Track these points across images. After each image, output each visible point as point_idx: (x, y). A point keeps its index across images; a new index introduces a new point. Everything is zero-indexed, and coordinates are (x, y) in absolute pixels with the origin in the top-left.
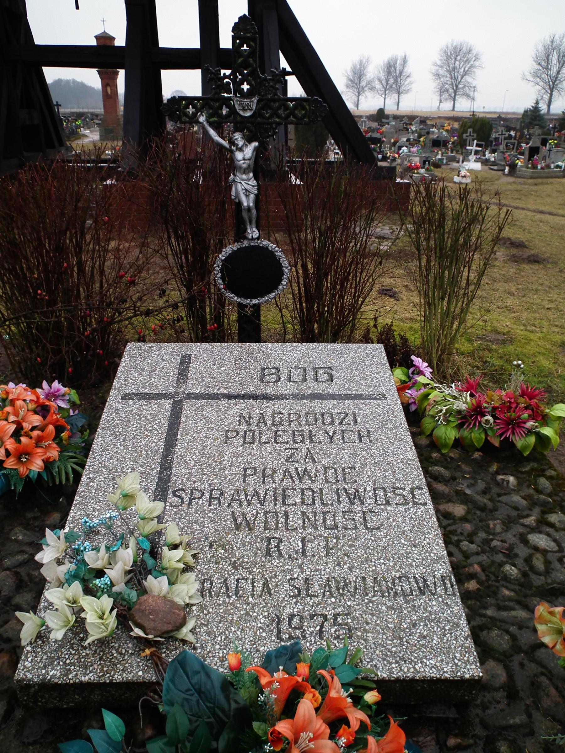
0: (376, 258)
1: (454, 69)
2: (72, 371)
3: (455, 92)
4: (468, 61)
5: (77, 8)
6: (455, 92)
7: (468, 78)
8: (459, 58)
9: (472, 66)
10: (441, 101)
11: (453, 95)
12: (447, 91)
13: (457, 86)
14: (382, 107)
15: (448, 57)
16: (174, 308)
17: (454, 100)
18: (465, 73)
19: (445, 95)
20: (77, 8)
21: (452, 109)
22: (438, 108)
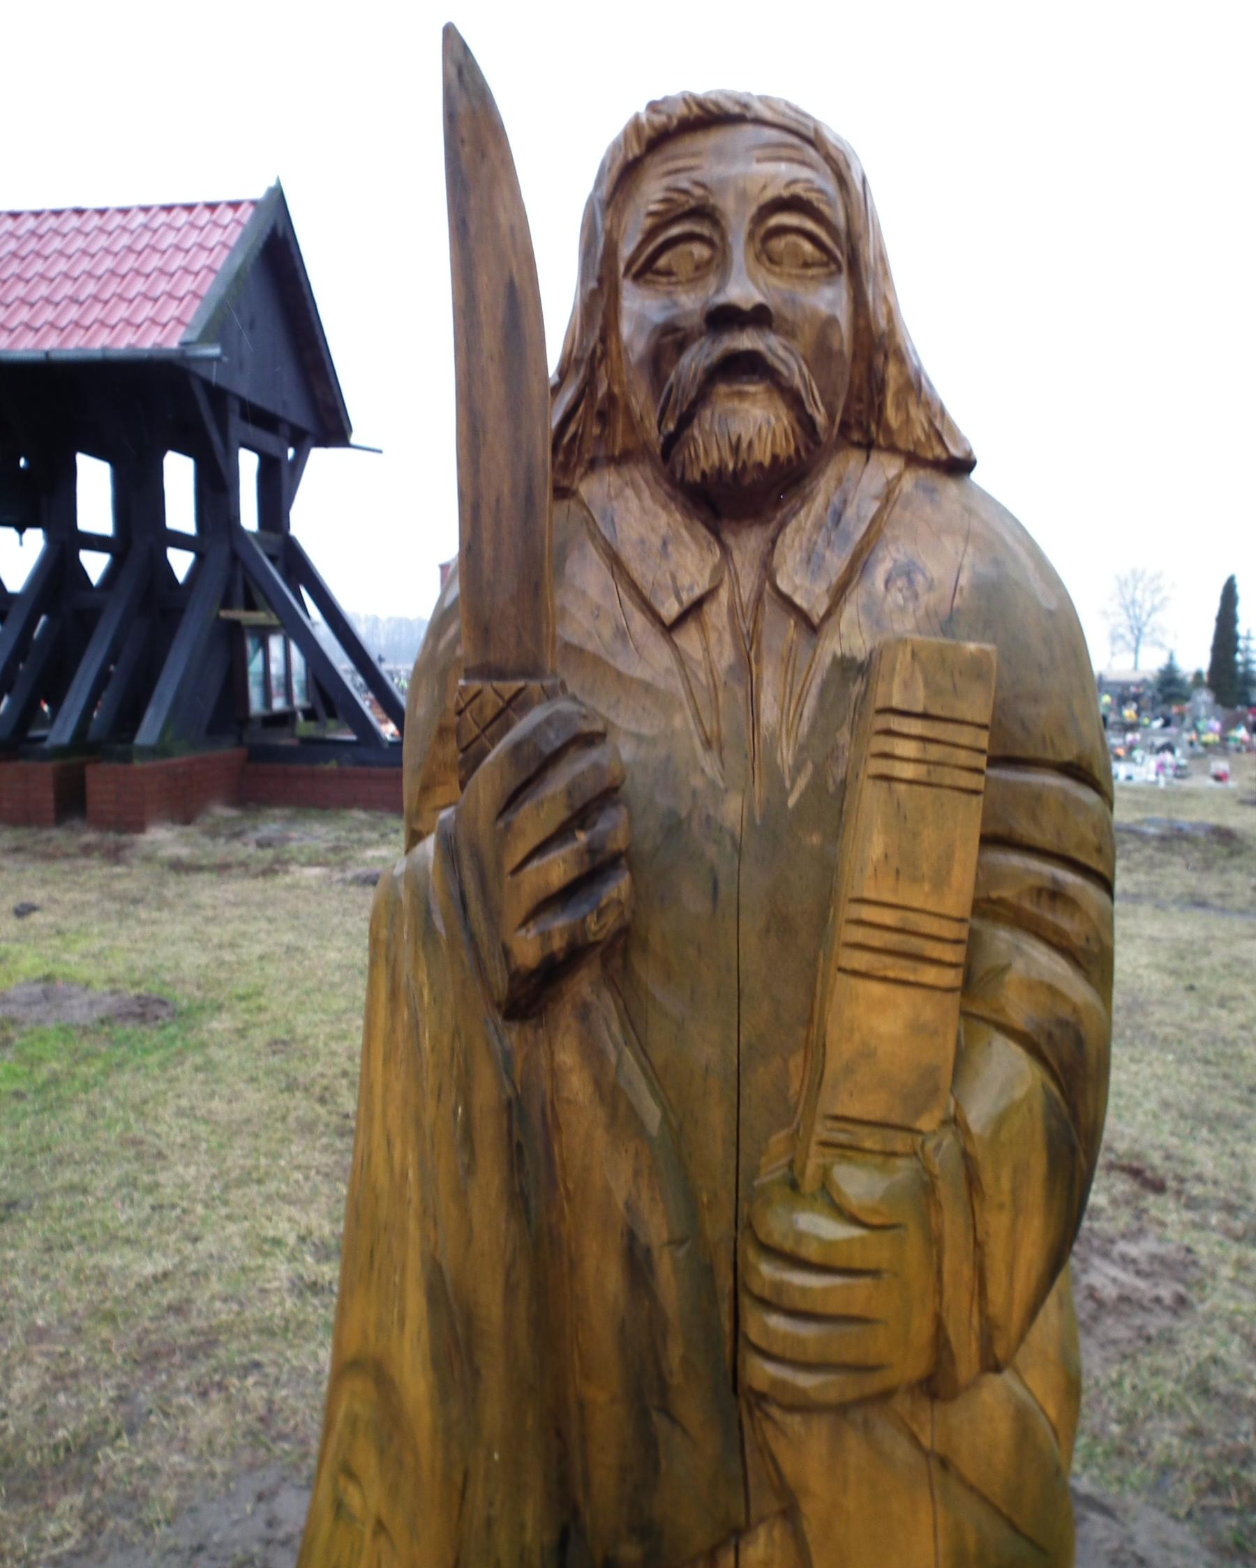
0: (762, 1372)
1: (1133, 602)
2: (1096, 700)
3: (1137, 641)
4: (1158, 590)
5: (380, 452)
6: (1137, 641)
7: (1156, 617)
8: (1140, 585)
9: (1166, 599)
10: (1113, 654)
11: (1133, 644)
12: (1122, 637)
13: (1140, 630)
14: (354, 440)
15: (1123, 584)
16: (99, 1284)
17: (1136, 651)
18: (1154, 609)
19: (1120, 644)
20: (380, 452)
21: (1131, 665)
22: (1109, 665)
